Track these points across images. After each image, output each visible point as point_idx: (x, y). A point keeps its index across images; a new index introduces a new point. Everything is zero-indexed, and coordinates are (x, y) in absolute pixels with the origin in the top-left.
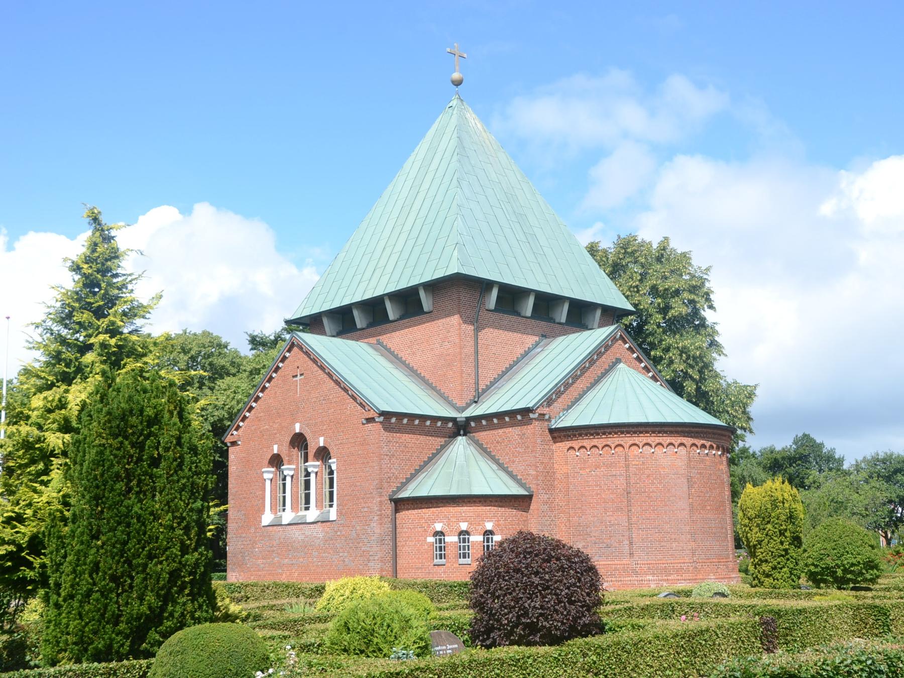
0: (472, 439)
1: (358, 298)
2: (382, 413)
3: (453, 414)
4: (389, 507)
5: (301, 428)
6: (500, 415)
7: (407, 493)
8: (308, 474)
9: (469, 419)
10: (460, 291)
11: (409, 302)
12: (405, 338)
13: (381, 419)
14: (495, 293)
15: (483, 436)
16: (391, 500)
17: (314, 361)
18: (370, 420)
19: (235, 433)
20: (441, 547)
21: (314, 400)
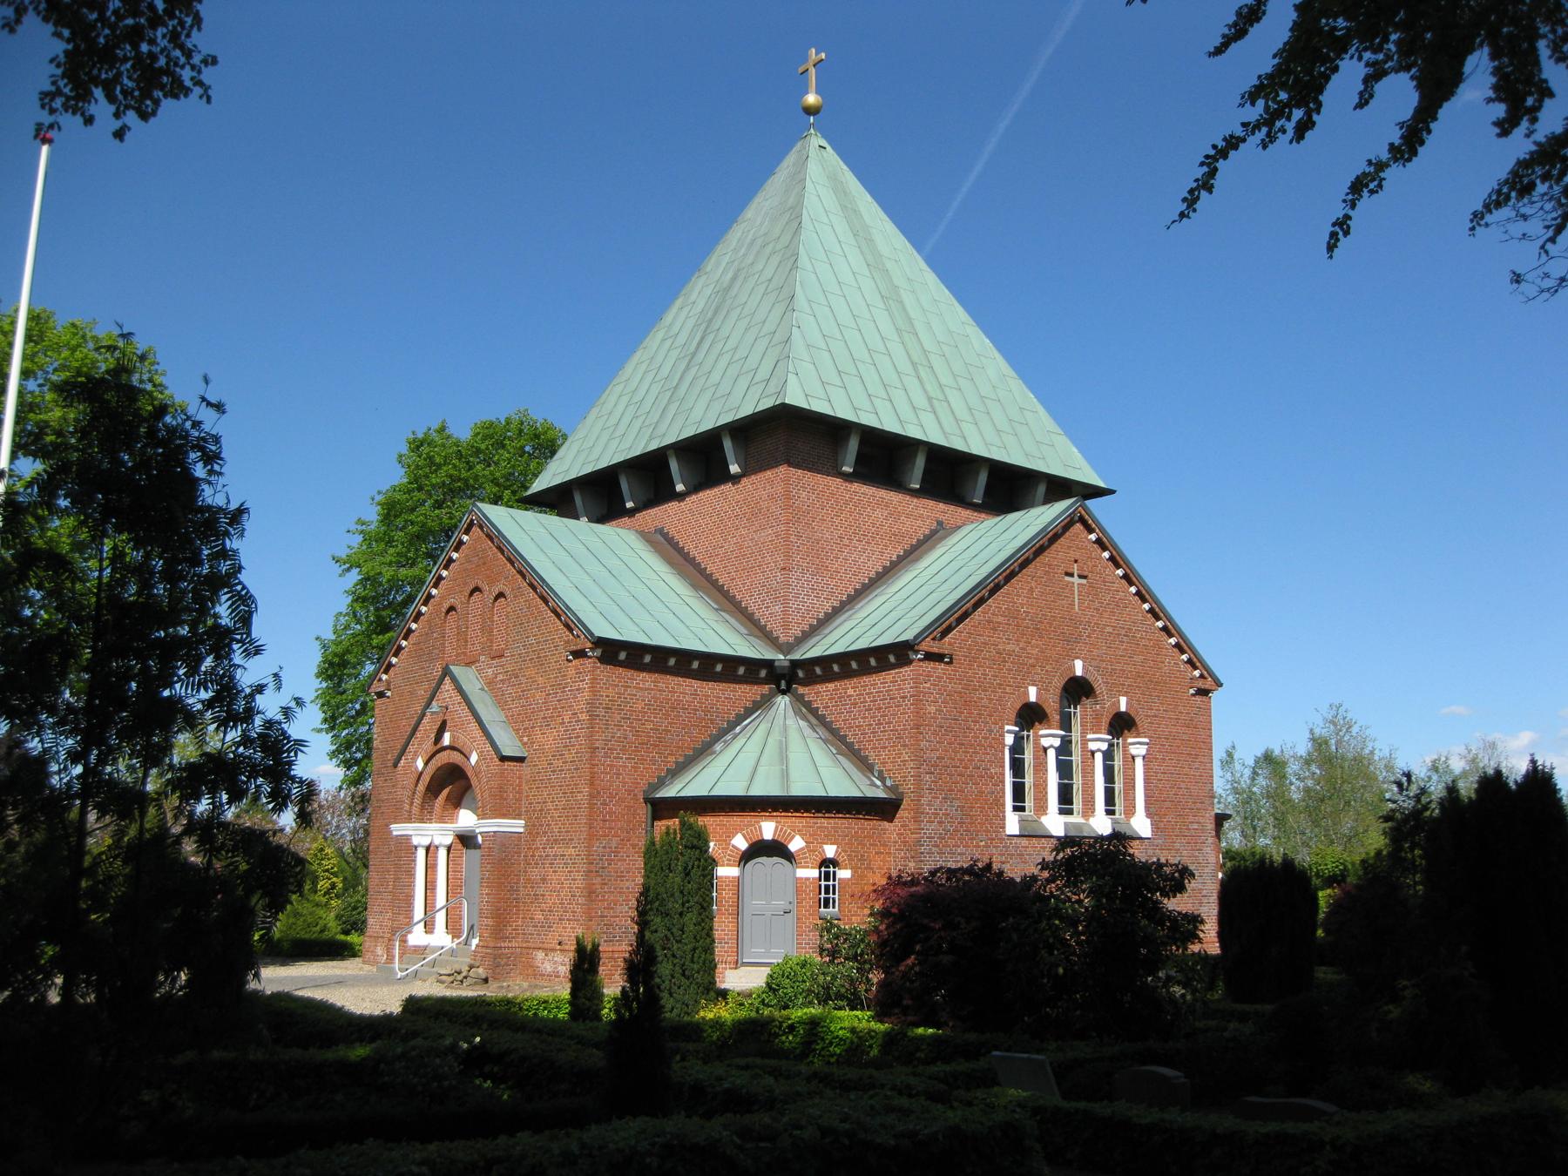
0: (799, 699)
1: (670, 439)
2: (600, 642)
3: (768, 654)
4: (644, 812)
5: (1038, 694)
6: (862, 655)
7: (670, 791)
8: (1065, 797)
9: (795, 664)
10: (790, 436)
11: (704, 459)
12: (695, 514)
13: (598, 653)
14: (853, 445)
15: (822, 694)
16: (646, 800)
17: (1040, 551)
18: (579, 654)
19: (384, 677)
20: (827, 887)
21: (1109, 629)
